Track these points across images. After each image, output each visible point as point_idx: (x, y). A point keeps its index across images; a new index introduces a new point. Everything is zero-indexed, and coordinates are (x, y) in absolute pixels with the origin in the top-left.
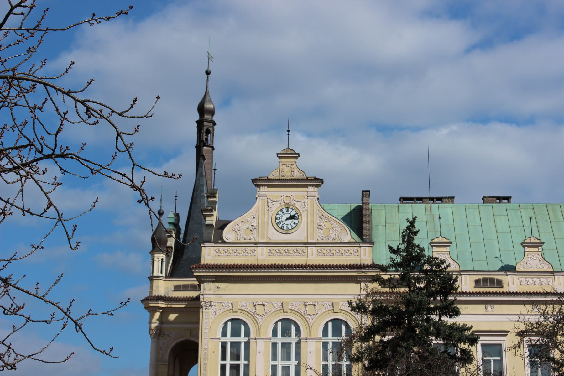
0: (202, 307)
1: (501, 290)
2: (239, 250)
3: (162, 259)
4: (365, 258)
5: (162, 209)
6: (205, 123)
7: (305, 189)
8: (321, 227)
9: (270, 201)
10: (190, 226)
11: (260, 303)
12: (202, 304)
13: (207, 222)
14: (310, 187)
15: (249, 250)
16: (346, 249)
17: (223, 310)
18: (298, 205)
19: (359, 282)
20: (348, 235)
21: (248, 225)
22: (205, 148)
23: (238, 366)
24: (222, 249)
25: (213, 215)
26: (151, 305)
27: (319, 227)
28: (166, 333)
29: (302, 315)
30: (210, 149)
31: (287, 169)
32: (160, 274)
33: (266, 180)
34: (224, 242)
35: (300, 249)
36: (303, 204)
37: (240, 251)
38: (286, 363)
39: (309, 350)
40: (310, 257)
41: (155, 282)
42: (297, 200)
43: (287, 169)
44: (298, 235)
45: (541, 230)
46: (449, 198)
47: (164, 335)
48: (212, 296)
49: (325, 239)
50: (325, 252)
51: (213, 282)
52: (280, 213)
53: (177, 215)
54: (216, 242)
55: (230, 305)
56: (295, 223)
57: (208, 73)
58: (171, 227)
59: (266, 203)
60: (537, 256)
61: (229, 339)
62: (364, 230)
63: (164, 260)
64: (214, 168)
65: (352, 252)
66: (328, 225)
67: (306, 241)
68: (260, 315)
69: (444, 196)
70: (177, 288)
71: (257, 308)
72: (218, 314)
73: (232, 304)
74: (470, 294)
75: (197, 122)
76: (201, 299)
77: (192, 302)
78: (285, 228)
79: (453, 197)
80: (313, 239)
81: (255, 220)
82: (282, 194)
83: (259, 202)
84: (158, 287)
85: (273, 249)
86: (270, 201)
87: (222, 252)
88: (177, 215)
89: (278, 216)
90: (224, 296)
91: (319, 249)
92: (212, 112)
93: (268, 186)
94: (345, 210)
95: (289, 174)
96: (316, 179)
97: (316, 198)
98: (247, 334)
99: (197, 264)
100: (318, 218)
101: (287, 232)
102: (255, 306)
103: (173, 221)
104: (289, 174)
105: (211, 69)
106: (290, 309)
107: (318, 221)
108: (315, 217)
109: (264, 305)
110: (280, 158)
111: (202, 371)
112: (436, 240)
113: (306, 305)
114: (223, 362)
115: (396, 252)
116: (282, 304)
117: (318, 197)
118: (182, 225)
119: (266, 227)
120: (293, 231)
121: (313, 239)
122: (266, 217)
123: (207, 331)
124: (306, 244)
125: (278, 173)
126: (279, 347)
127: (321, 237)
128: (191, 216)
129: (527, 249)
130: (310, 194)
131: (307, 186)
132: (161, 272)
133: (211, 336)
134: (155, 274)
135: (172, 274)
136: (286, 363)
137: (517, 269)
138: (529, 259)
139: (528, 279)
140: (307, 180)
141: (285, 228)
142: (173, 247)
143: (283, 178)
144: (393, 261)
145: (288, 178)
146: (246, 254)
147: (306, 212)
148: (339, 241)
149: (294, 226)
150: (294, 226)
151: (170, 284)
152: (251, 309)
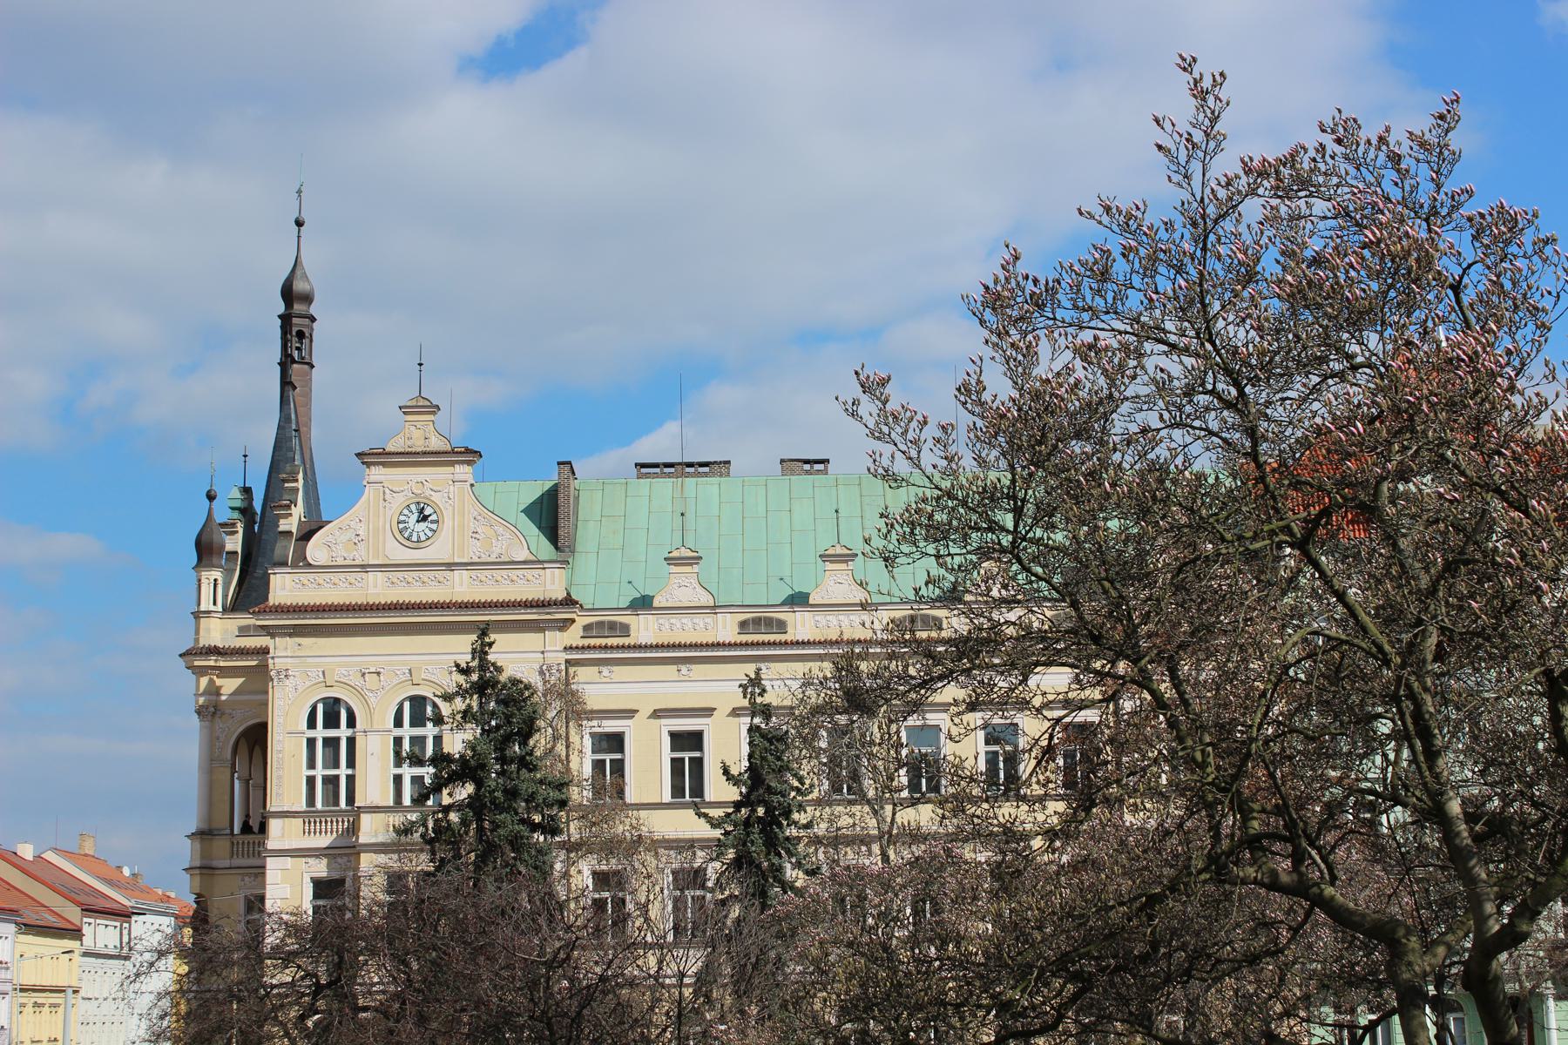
0: (272, 680)
1: (782, 638)
2: (335, 578)
3: (215, 580)
4: (553, 587)
5: (214, 488)
6: (295, 320)
7: (450, 469)
8: (477, 536)
9: (387, 491)
11: (373, 670)
12: (272, 673)
13: (281, 528)
14: (457, 466)
15: (351, 577)
16: (520, 573)
17: (308, 684)
18: (436, 497)
19: (542, 630)
21: (350, 535)
22: (295, 366)
23: (337, 777)
24: (305, 577)
25: (291, 515)
26: (196, 663)
27: (474, 535)
28: (227, 711)
29: (359, 693)
30: (306, 367)
31: (417, 434)
32: (212, 608)
33: (380, 454)
36: (446, 495)
37: (337, 581)
42: (435, 488)
43: (417, 434)
44: (437, 551)
46: (720, 462)
47: (223, 714)
48: (289, 660)
49: (483, 556)
50: (484, 579)
51: (290, 635)
52: (406, 512)
53: (247, 491)
54: (295, 565)
55: (321, 675)
56: (431, 530)
57: (299, 223)
58: (236, 515)
59: (382, 494)
60: (845, 578)
61: (320, 733)
62: (561, 532)
63: (220, 582)
64: (294, 427)
65: (530, 578)
66: (490, 532)
67: (452, 561)
69: (712, 460)
70: (244, 631)
71: (367, 679)
72: (300, 690)
73: (323, 672)
74: (731, 645)
75: (280, 317)
76: (271, 666)
78: (415, 538)
80: (463, 557)
81: (362, 524)
82: (411, 477)
83: (369, 493)
84: (208, 630)
85: (394, 576)
86: (387, 491)
87: (306, 582)
88: (247, 491)
89: (402, 518)
90: (309, 660)
92: (308, 298)
93: (384, 464)
94: (533, 491)
95: (421, 442)
96: (468, 451)
97: (468, 484)
99: (262, 606)
100: (472, 520)
101: (418, 544)
103: (238, 504)
104: (421, 442)
105: (305, 216)
106: (423, 680)
107: (472, 525)
108: (466, 516)
109: (378, 673)
111: (274, 788)
114: (311, 773)
115: (465, 671)
116: (410, 670)
117: (473, 482)
118: (258, 505)
119: (381, 538)
121: (463, 557)
122: (381, 519)
123: (281, 721)
124: (450, 566)
127: (478, 553)
128: (270, 495)
129: (829, 566)
130: (457, 477)
131: (452, 464)
132: (215, 604)
133: (289, 729)
134: (203, 608)
135: (234, 607)
137: (811, 601)
138: (832, 583)
139: (828, 618)
140: (453, 452)
141: (415, 538)
142: (240, 552)
143: (410, 450)
144: (460, 686)
145: (419, 450)
146: (347, 585)
148: (507, 560)
149: (430, 534)
150: (430, 534)
152: (356, 680)
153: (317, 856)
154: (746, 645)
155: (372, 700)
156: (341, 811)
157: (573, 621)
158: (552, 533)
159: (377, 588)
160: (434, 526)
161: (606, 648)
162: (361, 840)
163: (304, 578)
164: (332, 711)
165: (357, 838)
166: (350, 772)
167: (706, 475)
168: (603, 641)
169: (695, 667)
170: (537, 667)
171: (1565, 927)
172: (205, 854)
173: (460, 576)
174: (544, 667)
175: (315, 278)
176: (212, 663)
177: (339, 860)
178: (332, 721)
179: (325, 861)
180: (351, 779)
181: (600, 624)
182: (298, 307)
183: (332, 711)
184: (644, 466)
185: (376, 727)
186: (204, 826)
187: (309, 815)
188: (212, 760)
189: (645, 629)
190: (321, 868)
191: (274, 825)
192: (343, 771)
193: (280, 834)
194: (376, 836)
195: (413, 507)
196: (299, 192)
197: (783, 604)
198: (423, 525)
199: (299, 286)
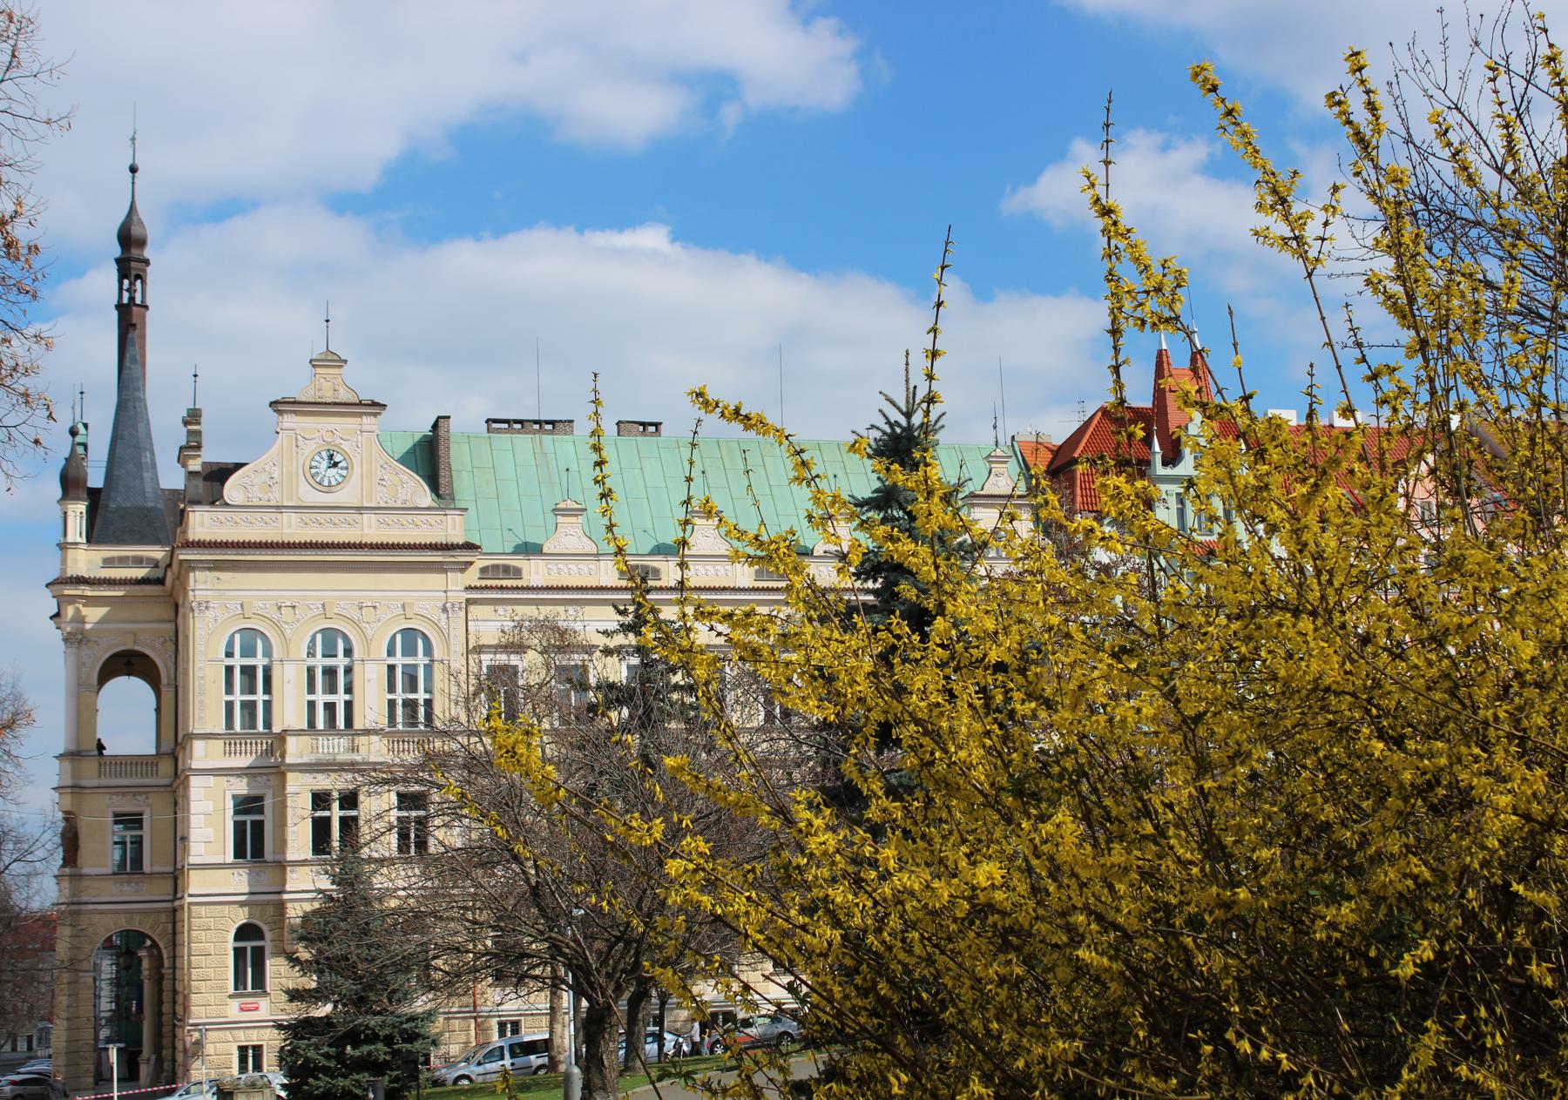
1: (519, 583)
2: (251, 517)
10: (117, 451)
11: (288, 604)
15: (266, 517)
17: (227, 615)
18: (345, 445)
19: (445, 571)
20: (416, 490)
21: (264, 477)
23: (254, 703)
26: (66, 592)
29: (356, 624)
32: (79, 540)
34: (227, 504)
35: (350, 518)
38: (330, 698)
39: (367, 676)
40: (366, 531)
41: (71, 553)
43: (326, 386)
44: (346, 495)
45: (712, 484)
48: (209, 593)
51: (210, 569)
52: (317, 458)
57: (133, 170)
62: (442, 481)
68: (287, 623)
70: (108, 563)
77: (138, 588)
78: (326, 483)
79: (572, 421)
84: (76, 561)
85: (307, 517)
86: (300, 438)
89: (314, 464)
90: (230, 593)
91: (381, 518)
92: (142, 243)
93: (296, 413)
96: (374, 404)
98: (268, 653)
102: (280, 608)
104: (330, 394)
109: (294, 607)
110: (314, 366)
111: (197, 711)
112: (562, 505)
113: (361, 608)
114: (392, 697)
116: (323, 605)
120: (339, 487)
124: (360, 509)
125: (312, 392)
126: (399, 710)
130: (365, 428)
131: (360, 415)
134: (70, 539)
136: (330, 698)
140: (360, 404)
141: (326, 483)
145: (329, 400)
147: (359, 457)
149: (340, 479)
150: (340, 479)
151: (98, 554)
152: (275, 614)
153: (238, 776)
154: (763, 589)
155: (288, 632)
156: (399, 732)
157: (471, 563)
158: (434, 482)
159: (291, 528)
160: (344, 472)
161: (502, 588)
162: (288, 760)
163: (221, 516)
164: (250, 638)
165: (283, 756)
166: (266, 697)
167: (518, 431)
168: (499, 583)
169: (587, 608)
170: (440, 604)
171: (6, 1013)
172: (75, 774)
173: (369, 519)
174: (448, 605)
175: (151, 224)
176: (79, 592)
177: (259, 779)
178: (410, 650)
179: (245, 780)
180: (349, 705)
181: (496, 567)
182: (134, 252)
183: (250, 638)
184: (496, 421)
185: (372, 657)
186: (73, 747)
187: (229, 736)
188: (79, 685)
189: (535, 572)
190: (242, 787)
191: (198, 746)
192: (260, 697)
193: (202, 754)
194: (302, 757)
195: (324, 454)
196: (133, 139)
197: (650, 554)
198: (333, 471)
199: (136, 231)
